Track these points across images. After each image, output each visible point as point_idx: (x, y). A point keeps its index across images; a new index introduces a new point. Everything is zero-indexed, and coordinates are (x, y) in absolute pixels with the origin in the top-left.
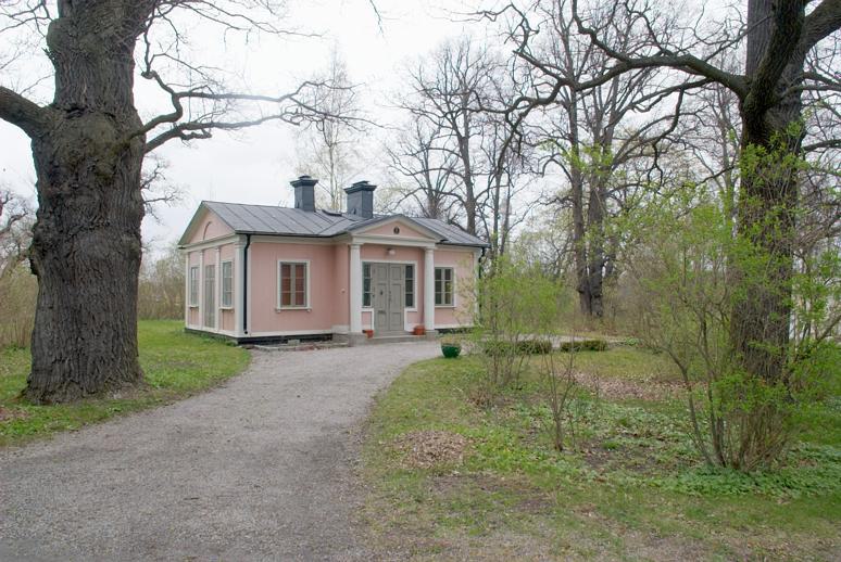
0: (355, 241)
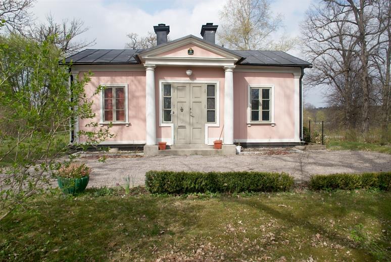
0: (147, 63)
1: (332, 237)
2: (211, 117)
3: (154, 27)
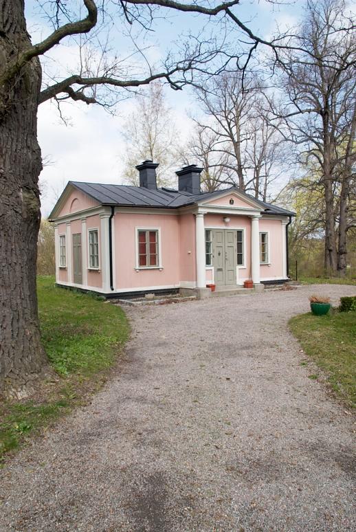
0: (200, 210)
1: (142, 400)
2: (240, 262)
3: (176, 173)
